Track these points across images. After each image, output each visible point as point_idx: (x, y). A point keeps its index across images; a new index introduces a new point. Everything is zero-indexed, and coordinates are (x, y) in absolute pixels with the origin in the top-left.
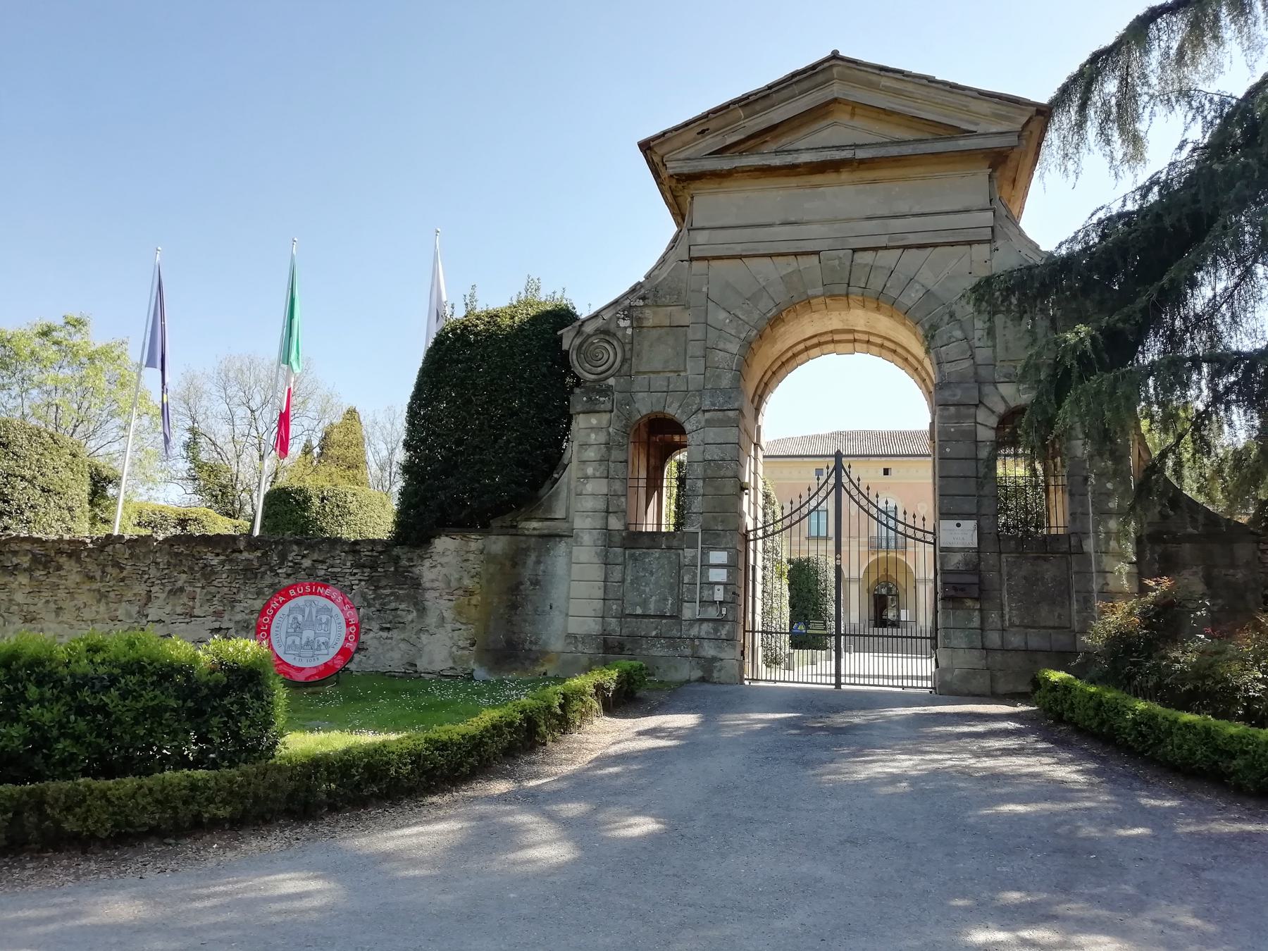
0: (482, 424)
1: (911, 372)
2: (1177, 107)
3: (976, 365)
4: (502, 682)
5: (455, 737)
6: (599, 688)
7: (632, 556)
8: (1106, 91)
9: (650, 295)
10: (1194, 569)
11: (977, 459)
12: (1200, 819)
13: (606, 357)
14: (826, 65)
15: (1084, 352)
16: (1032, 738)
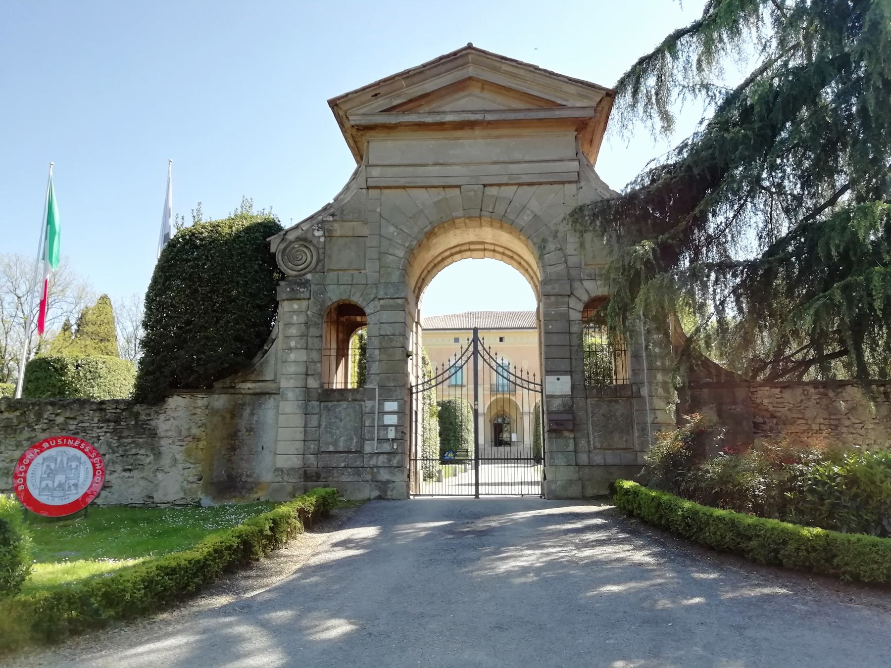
0: (206, 309)
1: (523, 271)
2: (699, 95)
3: (568, 268)
4: (223, 508)
5: (183, 563)
6: (301, 512)
7: (326, 407)
8: (648, 84)
9: (338, 213)
10: (711, 406)
11: (570, 333)
12: (735, 588)
13: (304, 258)
14: (464, 52)
15: (649, 259)
16: (614, 531)
